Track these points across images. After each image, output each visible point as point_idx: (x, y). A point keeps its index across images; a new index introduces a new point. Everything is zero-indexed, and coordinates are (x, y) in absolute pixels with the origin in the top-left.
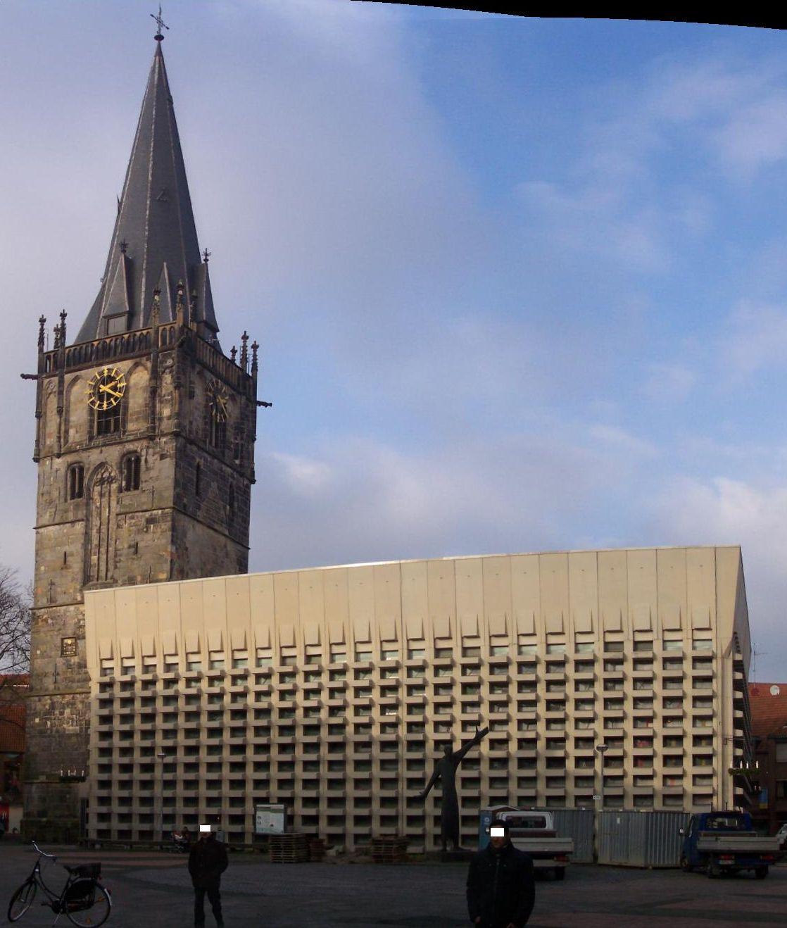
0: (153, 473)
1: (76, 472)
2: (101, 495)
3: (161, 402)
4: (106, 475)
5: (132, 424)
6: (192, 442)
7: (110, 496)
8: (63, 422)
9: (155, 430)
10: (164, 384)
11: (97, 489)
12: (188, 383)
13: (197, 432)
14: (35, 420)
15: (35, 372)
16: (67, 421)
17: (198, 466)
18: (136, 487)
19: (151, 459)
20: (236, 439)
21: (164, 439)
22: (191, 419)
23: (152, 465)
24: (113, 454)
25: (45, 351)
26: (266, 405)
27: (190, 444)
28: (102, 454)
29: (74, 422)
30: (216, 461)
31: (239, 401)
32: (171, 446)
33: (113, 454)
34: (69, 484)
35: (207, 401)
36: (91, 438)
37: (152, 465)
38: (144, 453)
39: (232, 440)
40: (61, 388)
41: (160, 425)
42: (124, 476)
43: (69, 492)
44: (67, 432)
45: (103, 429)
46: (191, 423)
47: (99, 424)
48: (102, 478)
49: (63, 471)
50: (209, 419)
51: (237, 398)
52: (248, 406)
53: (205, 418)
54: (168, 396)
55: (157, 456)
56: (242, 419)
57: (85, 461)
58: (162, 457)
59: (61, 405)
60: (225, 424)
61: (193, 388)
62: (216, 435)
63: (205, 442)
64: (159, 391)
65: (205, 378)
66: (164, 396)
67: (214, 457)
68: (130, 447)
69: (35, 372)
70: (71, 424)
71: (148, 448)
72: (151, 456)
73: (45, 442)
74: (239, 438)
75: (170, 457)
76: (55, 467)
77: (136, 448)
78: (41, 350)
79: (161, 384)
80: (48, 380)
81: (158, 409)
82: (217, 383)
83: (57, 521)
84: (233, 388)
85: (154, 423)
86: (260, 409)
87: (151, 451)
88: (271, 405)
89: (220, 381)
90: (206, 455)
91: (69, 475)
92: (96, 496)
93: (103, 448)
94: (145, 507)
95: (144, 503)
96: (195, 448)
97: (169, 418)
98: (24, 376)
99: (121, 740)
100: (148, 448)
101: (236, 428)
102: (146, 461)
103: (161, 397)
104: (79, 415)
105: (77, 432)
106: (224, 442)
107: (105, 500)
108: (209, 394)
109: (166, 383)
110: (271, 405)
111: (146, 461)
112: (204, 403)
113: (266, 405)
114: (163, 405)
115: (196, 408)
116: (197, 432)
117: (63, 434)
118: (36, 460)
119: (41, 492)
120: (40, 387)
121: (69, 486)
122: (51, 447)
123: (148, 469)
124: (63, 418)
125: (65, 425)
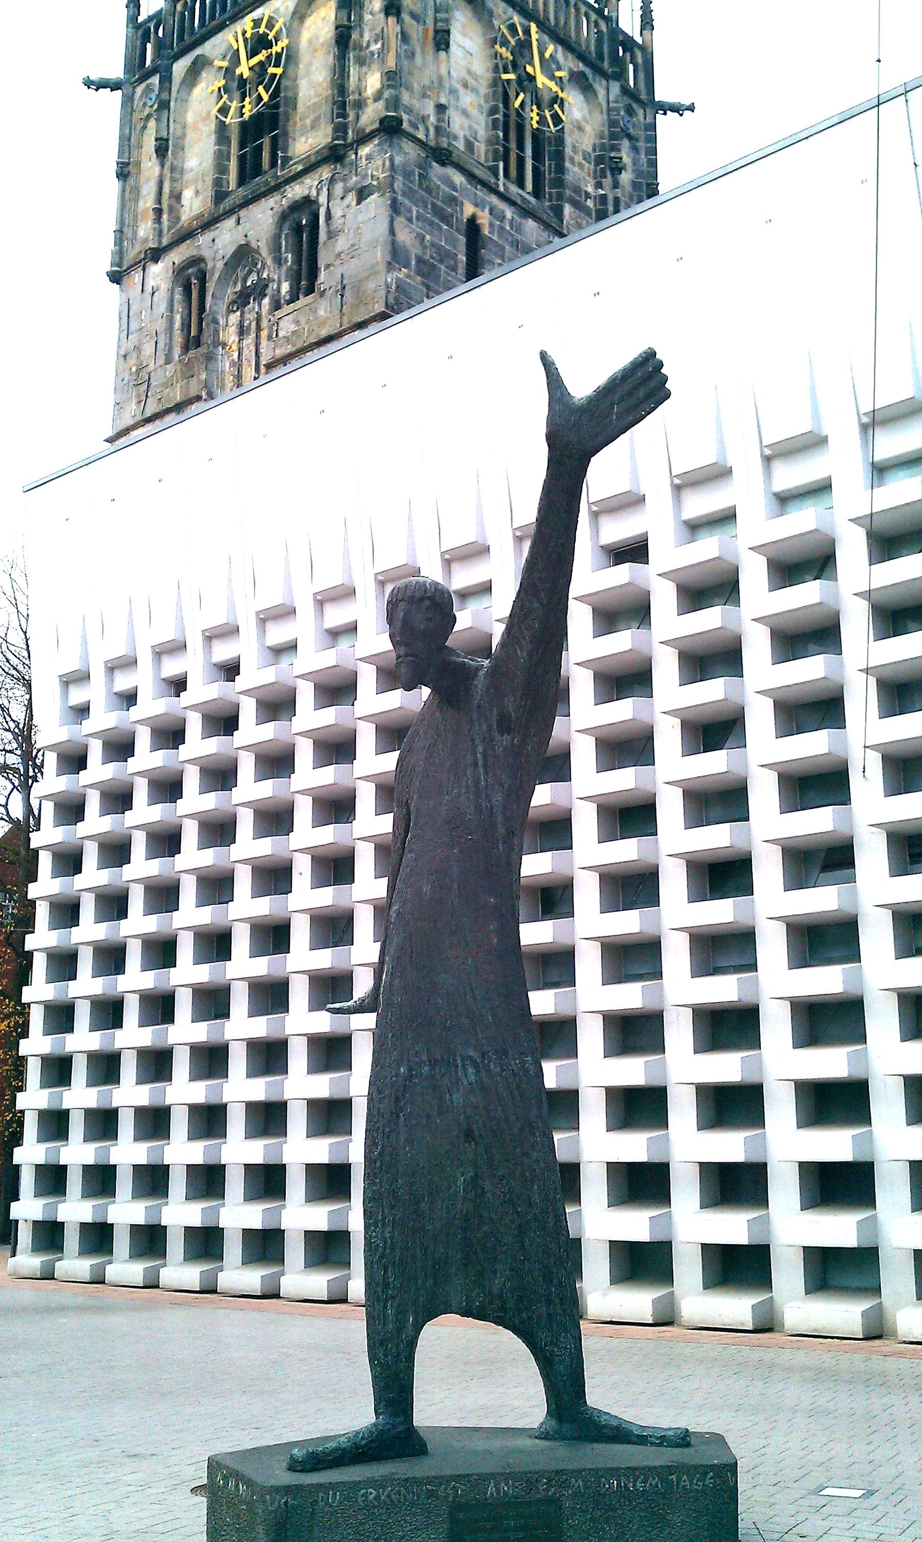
0: (342, 243)
1: (192, 281)
2: (242, 331)
3: (361, 62)
4: (252, 279)
5: (303, 139)
6: (443, 156)
7: (259, 329)
8: (167, 171)
9: (346, 133)
10: (367, 17)
11: (234, 318)
12: (431, 13)
13: (470, 146)
14: (115, 185)
15: (117, 71)
16: (177, 171)
17: (473, 227)
18: (310, 290)
19: (337, 212)
20: (599, 185)
21: (365, 151)
22: (443, 101)
23: (341, 221)
24: (260, 221)
25: (141, 19)
26: (677, 109)
27: (443, 164)
28: (240, 227)
29: (192, 170)
30: (531, 224)
31: (601, 93)
32: (380, 162)
33: (260, 221)
34: (178, 318)
35: (496, 69)
36: (220, 196)
37: (341, 221)
38: (323, 199)
39: (590, 189)
40: (165, 96)
41: (358, 117)
42: (284, 268)
43: (178, 339)
44: (177, 197)
45: (250, 168)
46: (441, 108)
47: (242, 159)
48: (244, 287)
49: (164, 286)
50: (508, 124)
51: (596, 86)
52: (630, 111)
53: (493, 111)
54: (376, 41)
55: (351, 198)
56: (613, 136)
57: (207, 253)
58: (362, 194)
59: (165, 135)
60: (559, 139)
61: (447, 21)
62: (535, 169)
63: (494, 171)
64: (355, 36)
65: (491, 14)
66: (368, 46)
67: (526, 212)
68: (296, 191)
69: (117, 71)
70: (188, 176)
71: (332, 181)
72: (338, 201)
73: (135, 233)
74: (608, 181)
75: (379, 188)
76: (151, 283)
77: (306, 192)
78: (133, 19)
79: (361, 19)
80: (143, 86)
81: (353, 81)
82: (527, 32)
83: (148, 414)
84: (581, 57)
85: (345, 116)
86: (665, 123)
87: (339, 188)
88: (691, 108)
89: (533, 27)
90: (494, 200)
91: (178, 297)
92: (230, 336)
93: (242, 213)
94: (324, 333)
95: (322, 324)
96: (458, 179)
97: (378, 97)
98: (88, 83)
99: (609, 1053)
100: (332, 181)
101: (599, 160)
102: (329, 216)
103: (361, 48)
104: (199, 155)
105: (197, 193)
106: (559, 182)
107: (249, 341)
108: (503, 51)
109: (371, 13)
110: (691, 108)
111: (329, 216)
112: (490, 75)
113: (677, 109)
114: (364, 69)
115: (465, 86)
116: (470, 146)
117: (167, 203)
118: (116, 278)
119: (122, 352)
120: (128, 101)
121: (177, 324)
122: (146, 240)
123: (331, 235)
124: (168, 165)
125: (173, 180)
